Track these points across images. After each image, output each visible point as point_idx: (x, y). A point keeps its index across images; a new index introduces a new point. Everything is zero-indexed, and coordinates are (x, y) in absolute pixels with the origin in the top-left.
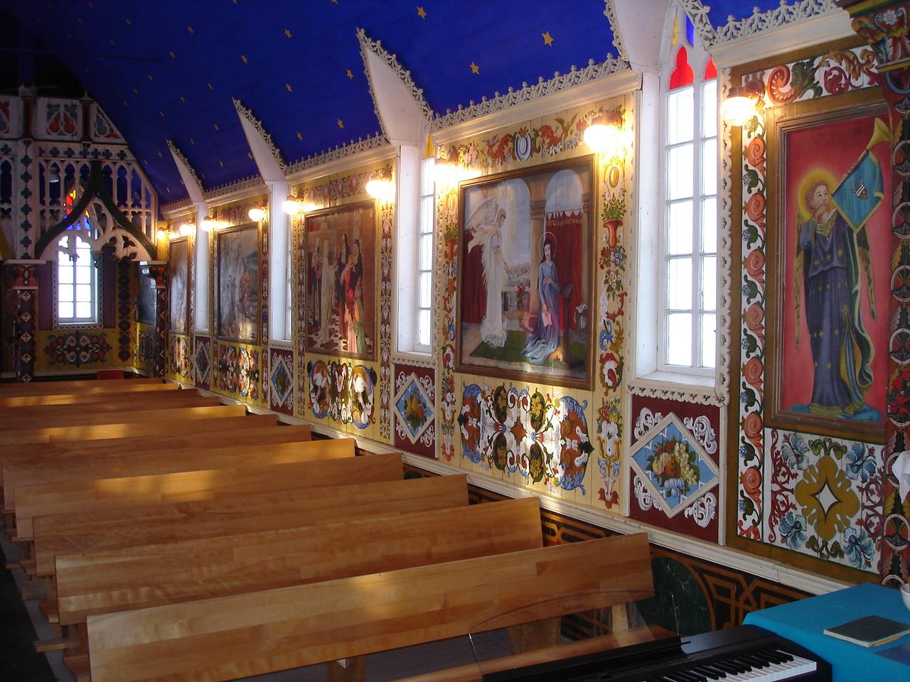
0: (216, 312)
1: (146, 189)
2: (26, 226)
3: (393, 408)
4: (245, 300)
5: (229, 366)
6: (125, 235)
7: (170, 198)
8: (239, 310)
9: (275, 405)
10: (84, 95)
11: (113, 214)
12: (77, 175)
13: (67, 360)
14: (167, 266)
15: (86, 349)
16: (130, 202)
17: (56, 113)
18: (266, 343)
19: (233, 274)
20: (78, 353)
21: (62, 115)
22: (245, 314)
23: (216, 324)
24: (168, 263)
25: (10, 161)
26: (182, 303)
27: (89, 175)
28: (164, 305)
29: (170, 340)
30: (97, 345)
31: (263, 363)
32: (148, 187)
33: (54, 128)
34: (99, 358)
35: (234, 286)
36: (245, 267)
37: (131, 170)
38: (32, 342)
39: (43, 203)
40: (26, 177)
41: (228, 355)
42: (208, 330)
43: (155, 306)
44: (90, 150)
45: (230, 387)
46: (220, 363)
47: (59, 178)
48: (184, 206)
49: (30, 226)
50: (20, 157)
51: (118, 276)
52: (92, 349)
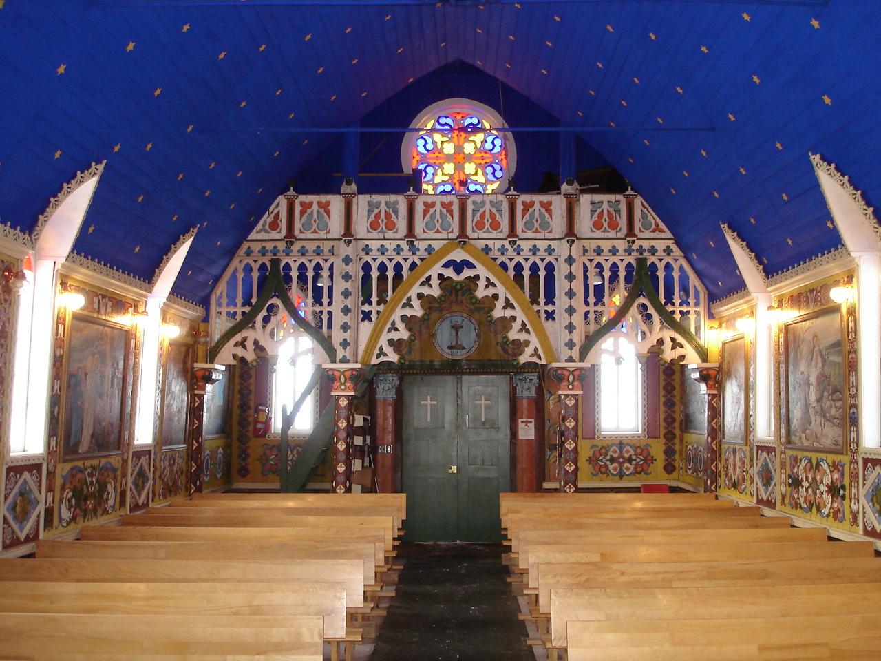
0: (784, 418)
1: (695, 286)
2: (570, 328)
3: (863, 501)
4: (824, 400)
5: (802, 480)
6: (673, 336)
7: (723, 287)
8: (817, 412)
9: (869, 529)
10: (627, 190)
11: (660, 314)
12: (622, 274)
13: (610, 471)
14: (719, 369)
15: (630, 460)
16: (677, 301)
17: (599, 210)
18: (856, 452)
19: (807, 370)
20: (621, 464)
21: (605, 212)
22: (824, 416)
23: (783, 431)
24: (720, 366)
25: (554, 262)
26: (739, 409)
27: (634, 273)
28: (716, 412)
29: (723, 451)
30: (641, 457)
31: (851, 476)
32: (697, 286)
33: (597, 225)
34: (643, 470)
35: (808, 384)
36: (824, 361)
37: (679, 266)
38: (575, 450)
39: (587, 303)
40: (570, 277)
41: (801, 468)
42: (773, 438)
43: (706, 414)
44: (635, 246)
45: (804, 505)
46: (790, 477)
47: (603, 278)
48: (740, 299)
49: (575, 328)
50: (565, 255)
51: (662, 384)
52: (635, 460)
